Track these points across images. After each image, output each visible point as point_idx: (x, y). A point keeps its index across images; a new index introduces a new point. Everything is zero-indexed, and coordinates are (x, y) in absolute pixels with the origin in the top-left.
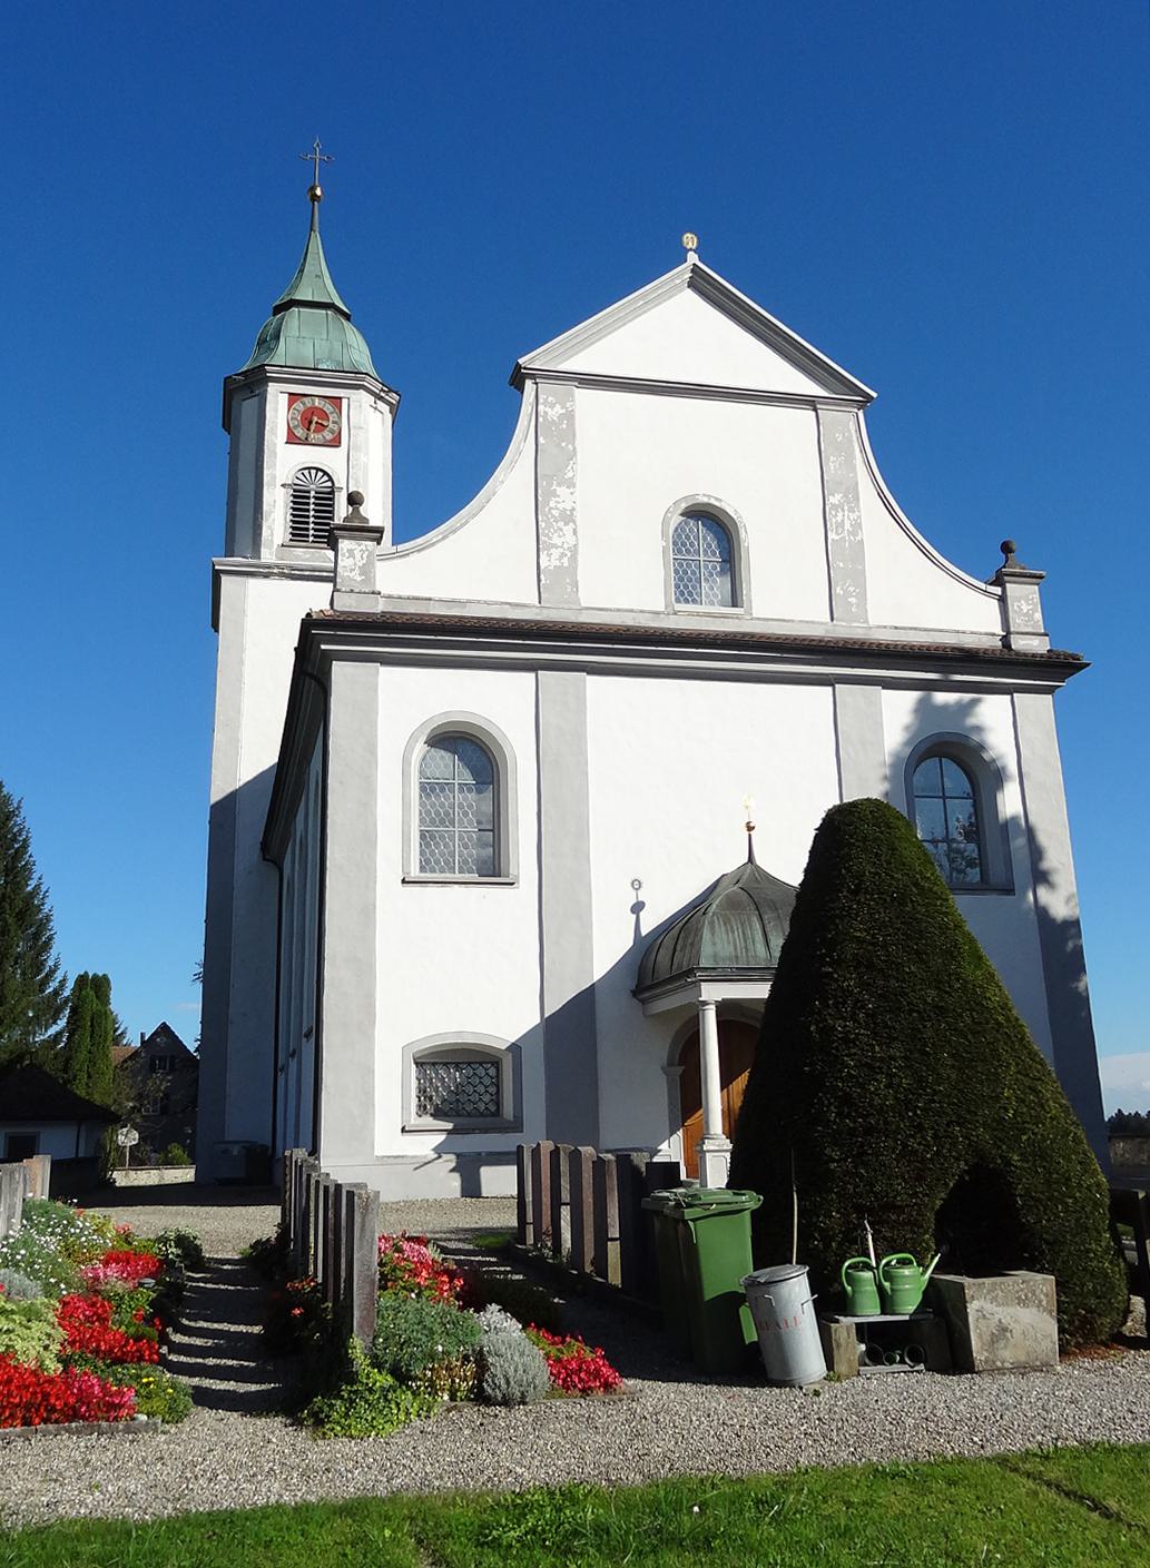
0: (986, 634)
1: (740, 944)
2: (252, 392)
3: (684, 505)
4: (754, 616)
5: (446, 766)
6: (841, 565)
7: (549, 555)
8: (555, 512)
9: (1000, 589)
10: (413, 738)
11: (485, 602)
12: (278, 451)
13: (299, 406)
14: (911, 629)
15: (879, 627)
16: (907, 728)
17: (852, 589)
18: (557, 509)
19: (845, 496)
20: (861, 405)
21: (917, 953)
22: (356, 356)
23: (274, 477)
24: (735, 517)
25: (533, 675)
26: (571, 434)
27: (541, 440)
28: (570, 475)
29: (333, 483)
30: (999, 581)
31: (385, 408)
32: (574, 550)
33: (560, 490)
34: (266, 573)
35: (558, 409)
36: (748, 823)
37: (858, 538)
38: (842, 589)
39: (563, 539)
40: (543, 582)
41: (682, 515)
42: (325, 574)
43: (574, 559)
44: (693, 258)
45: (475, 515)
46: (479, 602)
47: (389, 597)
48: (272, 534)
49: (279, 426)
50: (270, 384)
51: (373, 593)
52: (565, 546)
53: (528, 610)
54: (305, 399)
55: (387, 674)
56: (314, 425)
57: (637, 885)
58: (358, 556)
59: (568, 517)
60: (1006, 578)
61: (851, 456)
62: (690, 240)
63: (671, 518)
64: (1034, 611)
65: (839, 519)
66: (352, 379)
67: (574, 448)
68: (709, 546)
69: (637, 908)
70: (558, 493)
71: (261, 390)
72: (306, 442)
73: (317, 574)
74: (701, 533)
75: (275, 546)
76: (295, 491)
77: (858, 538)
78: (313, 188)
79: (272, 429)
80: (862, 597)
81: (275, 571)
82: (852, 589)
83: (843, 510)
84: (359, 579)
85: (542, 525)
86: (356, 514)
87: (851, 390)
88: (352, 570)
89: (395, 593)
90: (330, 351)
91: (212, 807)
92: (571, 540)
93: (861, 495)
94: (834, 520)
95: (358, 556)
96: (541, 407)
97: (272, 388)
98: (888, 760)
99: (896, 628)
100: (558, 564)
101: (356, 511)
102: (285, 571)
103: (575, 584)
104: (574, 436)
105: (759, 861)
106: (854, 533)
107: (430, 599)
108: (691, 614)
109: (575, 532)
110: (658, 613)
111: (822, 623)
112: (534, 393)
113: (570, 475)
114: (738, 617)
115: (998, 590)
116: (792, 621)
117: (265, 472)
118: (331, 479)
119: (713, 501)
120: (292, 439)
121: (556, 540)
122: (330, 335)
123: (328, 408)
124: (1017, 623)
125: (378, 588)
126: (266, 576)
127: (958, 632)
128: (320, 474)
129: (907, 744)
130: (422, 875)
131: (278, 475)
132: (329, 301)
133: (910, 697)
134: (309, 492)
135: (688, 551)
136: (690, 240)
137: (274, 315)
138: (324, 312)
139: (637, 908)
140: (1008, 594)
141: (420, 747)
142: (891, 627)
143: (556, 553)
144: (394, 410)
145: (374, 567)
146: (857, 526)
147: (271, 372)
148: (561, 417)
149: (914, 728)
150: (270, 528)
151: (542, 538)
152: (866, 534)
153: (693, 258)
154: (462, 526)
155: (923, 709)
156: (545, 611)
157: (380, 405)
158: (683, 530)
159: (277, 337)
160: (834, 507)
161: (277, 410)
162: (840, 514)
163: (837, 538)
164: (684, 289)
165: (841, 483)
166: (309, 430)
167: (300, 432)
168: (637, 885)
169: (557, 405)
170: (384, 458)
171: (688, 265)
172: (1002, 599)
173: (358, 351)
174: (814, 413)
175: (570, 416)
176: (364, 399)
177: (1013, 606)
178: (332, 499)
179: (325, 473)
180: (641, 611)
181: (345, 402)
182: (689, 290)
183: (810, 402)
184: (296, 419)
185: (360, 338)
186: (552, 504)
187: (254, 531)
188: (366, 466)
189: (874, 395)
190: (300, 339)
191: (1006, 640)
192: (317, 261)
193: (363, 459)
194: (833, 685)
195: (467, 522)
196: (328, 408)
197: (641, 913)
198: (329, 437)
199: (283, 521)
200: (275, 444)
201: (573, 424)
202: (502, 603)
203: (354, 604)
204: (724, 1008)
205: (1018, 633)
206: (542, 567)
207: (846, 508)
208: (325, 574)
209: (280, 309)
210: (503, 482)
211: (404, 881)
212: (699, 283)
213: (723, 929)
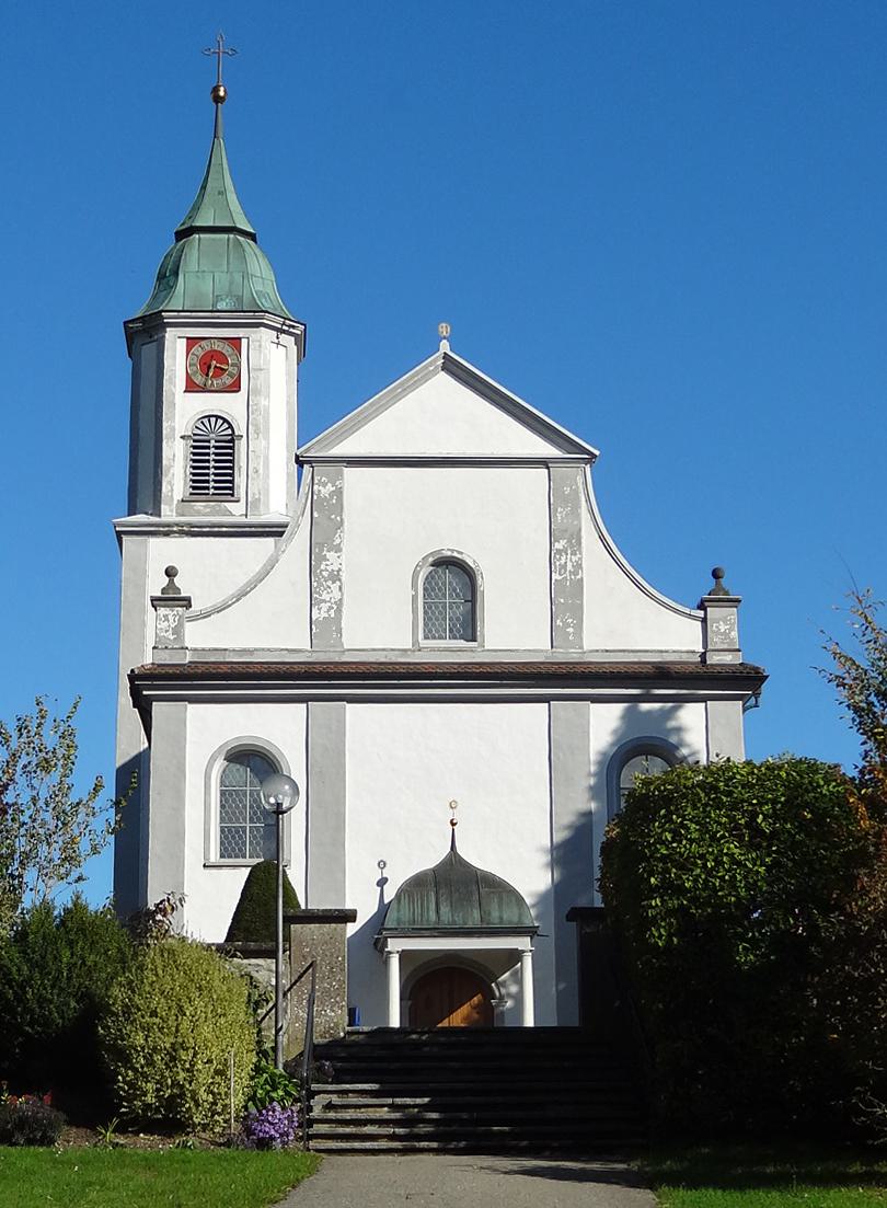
1: (418, 911)
3: (431, 559)
5: (241, 777)
6: (562, 601)
7: (319, 609)
9: (702, 612)
10: (213, 759)
11: (269, 650)
12: (176, 401)
13: (198, 351)
15: (592, 651)
16: (615, 732)
17: (570, 620)
19: (569, 541)
20: (587, 461)
23: (173, 429)
24: (473, 566)
27: (315, 515)
28: (338, 541)
29: (233, 431)
30: (702, 607)
31: (288, 340)
32: (340, 603)
34: (166, 531)
35: (330, 488)
36: (452, 820)
37: (579, 577)
38: (562, 621)
39: (331, 595)
40: (314, 631)
43: (339, 611)
44: (445, 346)
45: (261, 581)
46: (263, 649)
47: (195, 650)
48: (172, 490)
49: (177, 374)
50: (168, 329)
51: (182, 648)
52: (333, 601)
54: (203, 343)
55: (192, 708)
56: (215, 370)
57: (382, 865)
59: (335, 577)
60: (706, 604)
61: (577, 507)
62: (444, 329)
64: (731, 630)
65: (563, 562)
66: (253, 315)
67: (342, 519)
68: (455, 590)
69: (382, 882)
70: (328, 557)
72: (204, 389)
73: (216, 529)
74: (448, 576)
75: (175, 502)
76: (195, 441)
77: (579, 577)
78: (216, 89)
79: (170, 378)
80: (579, 627)
81: (175, 529)
82: (570, 620)
84: (172, 637)
85: (315, 584)
86: (171, 586)
88: (167, 631)
89: (199, 646)
90: (231, 284)
91: (119, 771)
92: (337, 595)
93: (583, 540)
94: (558, 563)
96: (316, 487)
97: (170, 333)
99: (607, 651)
101: (171, 582)
103: (340, 631)
106: (576, 573)
107: (226, 650)
109: (340, 588)
110: (405, 650)
111: (542, 651)
113: (338, 541)
114: (472, 650)
115: (701, 613)
116: (517, 650)
117: (165, 424)
118: (230, 426)
119: (455, 554)
120: (191, 387)
121: (325, 596)
122: (231, 266)
123: (227, 350)
125: (186, 645)
126: (166, 534)
128: (220, 421)
129: (613, 745)
130: (223, 860)
131: (177, 427)
132: (232, 225)
133: (618, 709)
135: (437, 596)
136: (444, 329)
137: (178, 240)
138: (226, 236)
139: (382, 882)
140: (708, 617)
141: (220, 764)
143: (325, 606)
144: (301, 342)
145: (183, 627)
146: (578, 566)
147: (168, 317)
148: (331, 494)
150: (170, 483)
151: (315, 595)
152: (585, 575)
153: (445, 346)
154: (252, 589)
155: (627, 717)
157: (283, 337)
159: (176, 274)
160: (559, 552)
161: (175, 357)
162: (563, 558)
163: (560, 578)
164: (434, 373)
165: (566, 531)
166: (207, 375)
167: (199, 379)
168: (382, 865)
169: (329, 485)
170: (289, 396)
171: (440, 354)
172: (704, 621)
173: (262, 279)
174: (546, 471)
175: (339, 492)
177: (713, 627)
178: (232, 448)
179: (225, 420)
181: (244, 342)
183: (543, 463)
184: (195, 365)
185: (264, 263)
186: (323, 567)
187: (155, 487)
188: (267, 410)
189: (597, 452)
190: (199, 274)
191: (703, 656)
192: (224, 178)
193: (263, 402)
195: (256, 586)
196: (227, 350)
197: (385, 887)
198: (228, 380)
199: (182, 476)
200: (174, 394)
201: (342, 500)
202: (282, 650)
203: (168, 658)
204: (405, 956)
205: (713, 650)
206: (314, 618)
208: (224, 529)
209: (183, 234)
210: (283, 552)
211: (204, 866)
212: (450, 366)
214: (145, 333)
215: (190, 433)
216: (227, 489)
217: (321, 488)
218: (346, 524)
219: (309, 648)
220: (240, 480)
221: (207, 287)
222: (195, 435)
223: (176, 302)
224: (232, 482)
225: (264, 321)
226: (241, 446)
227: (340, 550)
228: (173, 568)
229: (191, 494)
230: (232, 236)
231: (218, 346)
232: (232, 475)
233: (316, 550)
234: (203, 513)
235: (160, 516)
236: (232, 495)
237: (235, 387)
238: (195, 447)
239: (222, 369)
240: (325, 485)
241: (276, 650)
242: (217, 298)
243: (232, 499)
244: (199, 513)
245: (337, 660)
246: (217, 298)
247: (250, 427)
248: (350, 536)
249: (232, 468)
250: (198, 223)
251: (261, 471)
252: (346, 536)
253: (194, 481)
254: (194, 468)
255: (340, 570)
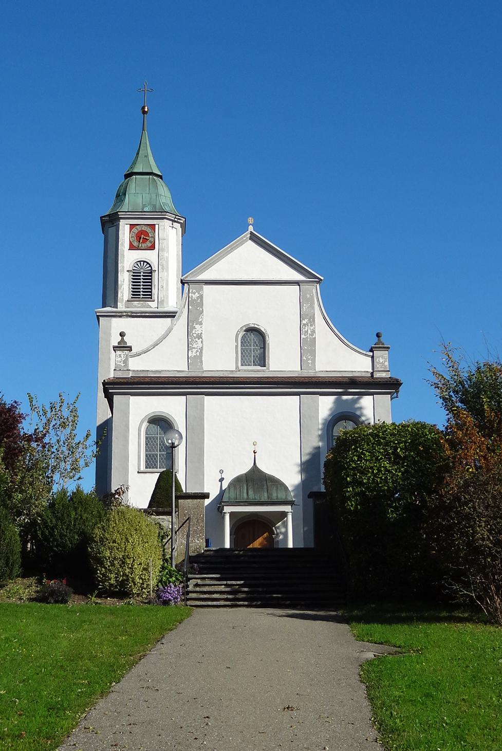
0: (365, 372)
1: (238, 493)
2: (113, 224)
3: (244, 328)
4: (270, 370)
6: (306, 348)
8: (195, 335)
11: (168, 371)
13: (135, 230)
14: (333, 371)
16: (331, 409)
18: (195, 333)
19: (309, 320)
20: (317, 282)
21: (167, 500)
22: (163, 200)
23: (123, 267)
25: (185, 397)
26: (202, 304)
27: (190, 307)
28: (201, 320)
29: (151, 268)
30: (371, 351)
31: (177, 226)
32: (201, 349)
33: (196, 326)
34: (120, 315)
35: (197, 295)
40: (189, 362)
41: (245, 331)
42: (147, 314)
43: (201, 352)
44: (251, 228)
46: (166, 371)
47: (134, 371)
48: (123, 296)
50: (121, 220)
51: (128, 370)
52: (198, 348)
53: (184, 373)
54: (137, 227)
56: (143, 240)
57: (221, 472)
58: (122, 357)
59: (199, 336)
60: (374, 349)
61: (313, 303)
62: (251, 220)
63: (239, 334)
65: (306, 329)
66: (160, 214)
69: (221, 480)
71: (117, 223)
72: (138, 249)
73: (144, 314)
74: (252, 336)
75: (124, 302)
76: (133, 273)
78: (143, 108)
79: (122, 243)
80: (314, 360)
81: (124, 314)
83: (308, 326)
84: (123, 365)
85: (190, 340)
86: (122, 341)
87: (312, 277)
88: (120, 362)
89: (136, 369)
91: (98, 427)
93: (316, 319)
94: (304, 330)
95: (122, 357)
96: (190, 294)
97: (122, 222)
98: (320, 427)
99: (327, 371)
100: (195, 355)
102: (129, 314)
103: (202, 362)
104: (203, 305)
105: (258, 465)
106: (312, 335)
107: (148, 371)
108: (245, 371)
109: (202, 342)
110: (233, 371)
112: (188, 289)
113: (201, 320)
114: (263, 371)
115: (371, 354)
117: (119, 265)
118: (150, 266)
119: (256, 326)
120: (132, 247)
121: (195, 346)
122: (150, 191)
123: (148, 230)
124: (378, 367)
125: (130, 369)
126: (120, 317)
127: (353, 372)
128: (145, 264)
129: (330, 415)
130: (147, 469)
131: (125, 266)
132: (151, 171)
133: (332, 398)
134: (140, 273)
136: (251, 220)
137: (126, 179)
138: (148, 176)
139: (221, 480)
141: (145, 424)
142: (325, 371)
143: (194, 350)
144: (183, 226)
146: (313, 332)
147: (121, 215)
149: (333, 409)
150: (122, 292)
151: (190, 345)
152: (317, 335)
153: (251, 228)
155: (337, 402)
156: (190, 373)
157: (175, 224)
158: (245, 337)
159: (125, 194)
160: (304, 325)
162: (306, 328)
164: (246, 241)
166: (139, 242)
167: (135, 244)
168: (221, 472)
169: (197, 293)
170: (177, 252)
172: (373, 357)
174: (299, 287)
175: (201, 297)
176: (166, 224)
177: (376, 360)
178: (151, 276)
179: (148, 263)
180: (226, 371)
181: (157, 226)
182: (250, 241)
183: (297, 283)
184: (133, 237)
185: (166, 189)
186: (194, 332)
188: (167, 258)
189: (322, 278)
191: (372, 373)
193: (166, 255)
194: (300, 395)
195: (162, 341)
196: (148, 230)
197: (223, 482)
198: (149, 244)
203: (121, 374)
204: (232, 514)
205: (377, 371)
206: (189, 356)
207: (309, 325)
208: (147, 314)
209: (128, 176)
210: (175, 325)
211: (138, 472)
212: (253, 238)
213: (233, 488)
214: (110, 222)
215: (131, 269)
216: (149, 295)
217: (193, 295)
218: (204, 312)
219: (187, 370)
220: (155, 291)
221: (139, 200)
222: (133, 270)
223: (125, 208)
224: (151, 292)
225: (166, 216)
226: (155, 275)
227: (202, 324)
228: (123, 332)
229: (132, 298)
230: (151, 177)
231: (144, 228)
232: (151, 289)
233: (190, 324)
234: (138, 306)
235: (117, 308)
236: (151, 298)
237: (152, 248)
238: (133, 276)
239: (147, 239)
240: (194, 293)
241: (172, 371)
242: (144, 206)
243: (151, 300)
244: (135, 307)
245: (200, 375)
246: (144, 206)
247: (159, 266)
248: (206, 318)
249: (151, 286)
250: (135, 170)
251: (165, 287)
252: (204, 317)
253: (133, 292)
254: (133, 285)
255: (202, 333)
